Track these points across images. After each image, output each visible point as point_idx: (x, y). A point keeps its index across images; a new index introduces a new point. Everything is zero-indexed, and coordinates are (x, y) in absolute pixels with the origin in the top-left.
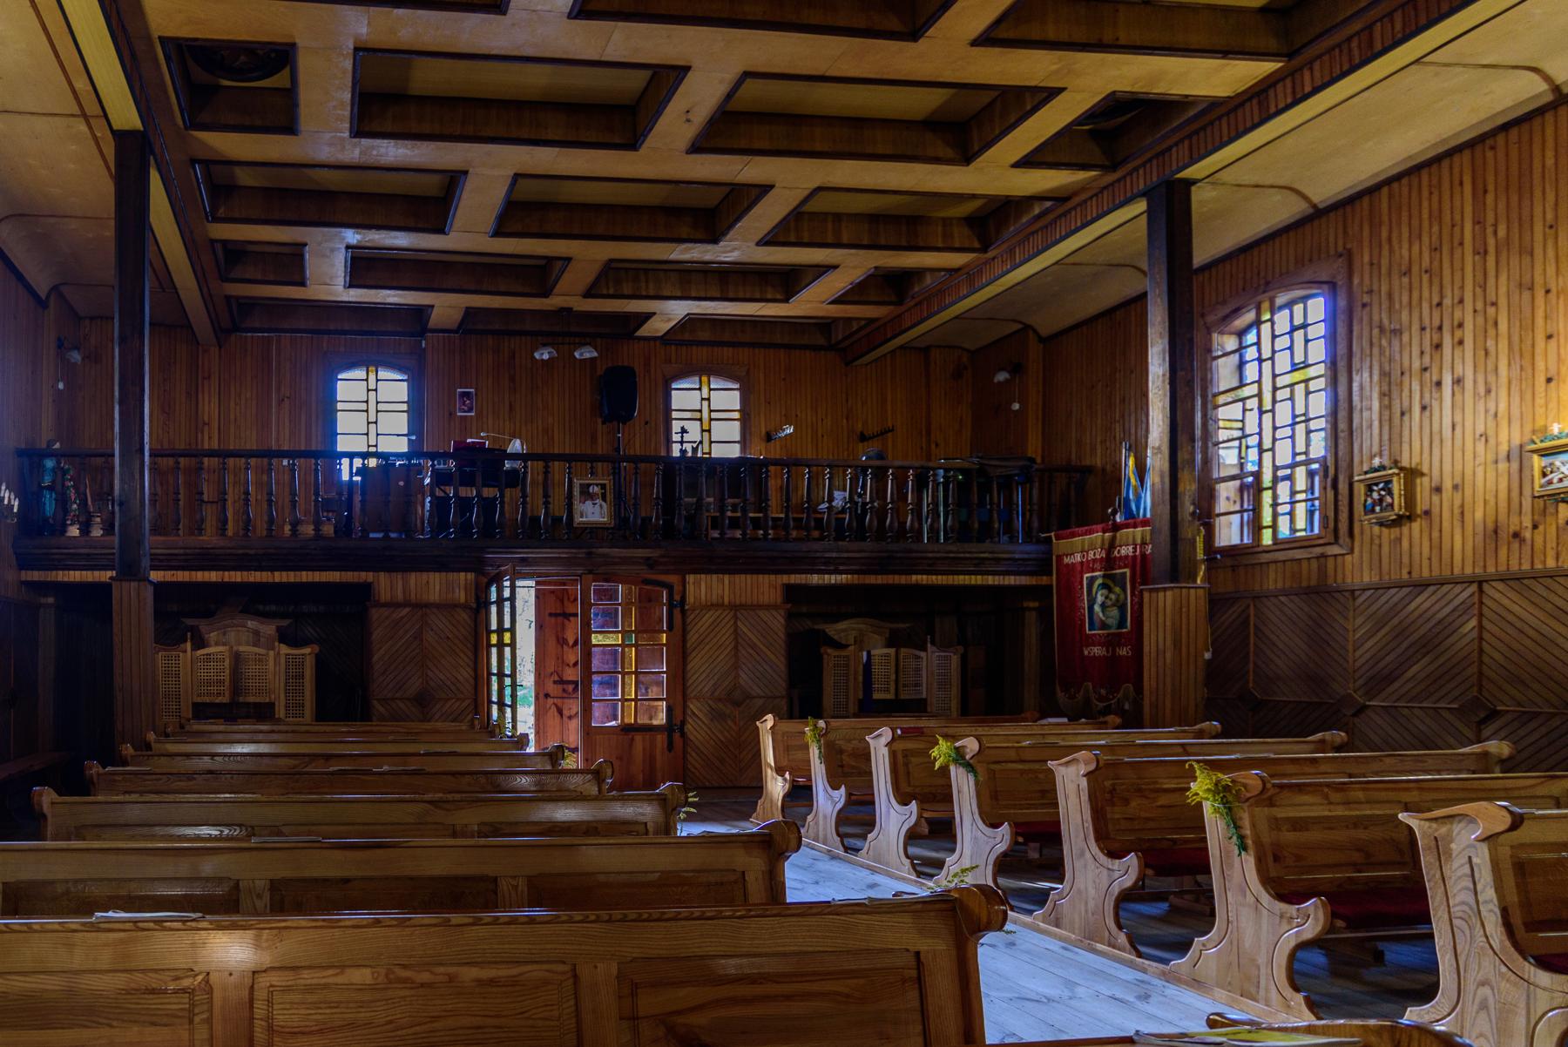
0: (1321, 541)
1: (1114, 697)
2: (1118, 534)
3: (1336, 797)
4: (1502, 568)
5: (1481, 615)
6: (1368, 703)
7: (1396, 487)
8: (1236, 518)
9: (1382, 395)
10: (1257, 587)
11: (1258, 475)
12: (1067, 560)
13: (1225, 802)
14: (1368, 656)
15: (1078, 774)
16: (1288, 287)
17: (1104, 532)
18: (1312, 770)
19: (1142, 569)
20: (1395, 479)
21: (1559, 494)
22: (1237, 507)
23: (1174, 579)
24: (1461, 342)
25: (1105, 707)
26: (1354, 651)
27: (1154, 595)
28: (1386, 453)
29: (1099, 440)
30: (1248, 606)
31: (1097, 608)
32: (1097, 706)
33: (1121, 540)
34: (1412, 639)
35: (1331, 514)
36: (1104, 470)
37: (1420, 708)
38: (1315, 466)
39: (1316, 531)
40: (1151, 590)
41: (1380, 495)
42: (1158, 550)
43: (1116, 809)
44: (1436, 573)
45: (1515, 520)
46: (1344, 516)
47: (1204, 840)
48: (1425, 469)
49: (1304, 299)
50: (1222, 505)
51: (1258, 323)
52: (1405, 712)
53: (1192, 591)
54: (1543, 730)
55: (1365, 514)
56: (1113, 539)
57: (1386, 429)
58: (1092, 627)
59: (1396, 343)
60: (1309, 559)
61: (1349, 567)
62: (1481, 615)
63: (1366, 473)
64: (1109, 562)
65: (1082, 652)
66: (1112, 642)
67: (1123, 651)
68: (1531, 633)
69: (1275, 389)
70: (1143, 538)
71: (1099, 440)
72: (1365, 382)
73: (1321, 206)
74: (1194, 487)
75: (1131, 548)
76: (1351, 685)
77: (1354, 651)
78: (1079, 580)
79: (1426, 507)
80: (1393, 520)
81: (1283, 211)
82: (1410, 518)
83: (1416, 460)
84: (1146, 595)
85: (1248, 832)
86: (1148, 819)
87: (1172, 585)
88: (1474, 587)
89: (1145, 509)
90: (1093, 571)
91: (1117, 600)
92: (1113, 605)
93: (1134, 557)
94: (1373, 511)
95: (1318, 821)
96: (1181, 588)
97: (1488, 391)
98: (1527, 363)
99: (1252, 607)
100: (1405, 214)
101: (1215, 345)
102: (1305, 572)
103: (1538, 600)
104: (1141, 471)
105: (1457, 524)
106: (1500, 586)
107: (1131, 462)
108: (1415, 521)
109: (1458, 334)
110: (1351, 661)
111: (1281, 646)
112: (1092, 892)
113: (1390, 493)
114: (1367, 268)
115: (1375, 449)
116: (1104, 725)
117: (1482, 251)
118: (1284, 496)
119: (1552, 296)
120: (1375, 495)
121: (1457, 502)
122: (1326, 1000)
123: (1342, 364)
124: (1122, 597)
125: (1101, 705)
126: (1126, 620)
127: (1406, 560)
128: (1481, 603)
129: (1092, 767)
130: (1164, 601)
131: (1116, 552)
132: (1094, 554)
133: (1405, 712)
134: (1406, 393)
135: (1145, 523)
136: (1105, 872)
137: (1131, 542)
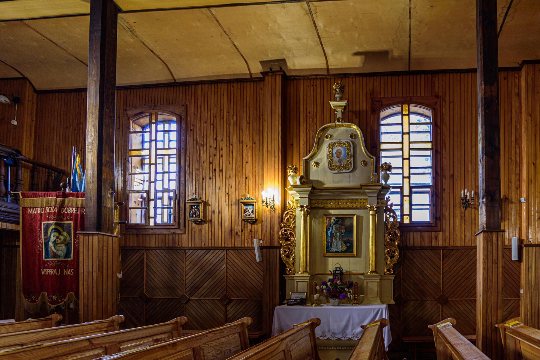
0: (173, 227)
1: (62, 301)
2: (66, 199)
4: (233, 245)
6: (190, 298)
7: (201, 208)
11: (148, 192)
12: (30, 211)
16: (164, 111)
17: (57, 197)
18: (173, 351)
20: (200, 205)
21: (249, 220)
22: (140, 206)
24: (222, 156)
26: (186, 276)
27: (86, 238)
28: (197, 193)
30: (144, 254)
31: (51, 244)
32: (50, 307)
33: (68, 203)
35: (177, 215)
37: (208, 299)
38: (171, 194)
39: (172, 222)
41: (195, 210)
42: (91, 212)
44: (213, 245)
45: (236, 227)
46: (182, 218)
48: (210, 203)
50: (133, 205)
51: (151, 123)
52: (203, 301)
53: (110, 238)
54: (244, 306)
55: (190, 218)
56: (63, 202)
57: (197, 183)
58: (47, 256)
60: (169, 234)
61: (184, 239)
62: (227, 263)
63: (190, 200)
64: (60, 216)
66: (60, 266)
67: (69, 272)
68: (241, 270)
69: (156, 155)
70: (82, 204)
73: (177, 81)
75: (74, 209)
76: (184, 291)
77: (186, 276)
78: (38, 225)
79: (210, 218)
80: (199, 222)
81: (162, 77)
83: (207, 199)
84: (81, 237)
87: (97, 232)
88: (225, 252)
91: (65, 240)
92: (62, 243)
94: (193, 216)
96: (103, 235)
97: (230, 177)
99: (145, 254)
100: (206, 99)
102: (167, 241)
103: (243, 258)
107: (78, 159)
108: (207, 223)
109: (221, 152)
110: (184, 280)
111: (158, 273)
113: (198, 210)
114: (193, 115)
115: (194, 191)
117: (229, 124)
119: (248, 147)
120: (193, 210)
124: (68, 238)
125: (53, 306)
126: (71, 252)
127: (203, 238)
128: (227, 258)
131: (65, 210)
132: (50, 210)
133: (203, 301)
135: (83, 195)
137: (74, 205)
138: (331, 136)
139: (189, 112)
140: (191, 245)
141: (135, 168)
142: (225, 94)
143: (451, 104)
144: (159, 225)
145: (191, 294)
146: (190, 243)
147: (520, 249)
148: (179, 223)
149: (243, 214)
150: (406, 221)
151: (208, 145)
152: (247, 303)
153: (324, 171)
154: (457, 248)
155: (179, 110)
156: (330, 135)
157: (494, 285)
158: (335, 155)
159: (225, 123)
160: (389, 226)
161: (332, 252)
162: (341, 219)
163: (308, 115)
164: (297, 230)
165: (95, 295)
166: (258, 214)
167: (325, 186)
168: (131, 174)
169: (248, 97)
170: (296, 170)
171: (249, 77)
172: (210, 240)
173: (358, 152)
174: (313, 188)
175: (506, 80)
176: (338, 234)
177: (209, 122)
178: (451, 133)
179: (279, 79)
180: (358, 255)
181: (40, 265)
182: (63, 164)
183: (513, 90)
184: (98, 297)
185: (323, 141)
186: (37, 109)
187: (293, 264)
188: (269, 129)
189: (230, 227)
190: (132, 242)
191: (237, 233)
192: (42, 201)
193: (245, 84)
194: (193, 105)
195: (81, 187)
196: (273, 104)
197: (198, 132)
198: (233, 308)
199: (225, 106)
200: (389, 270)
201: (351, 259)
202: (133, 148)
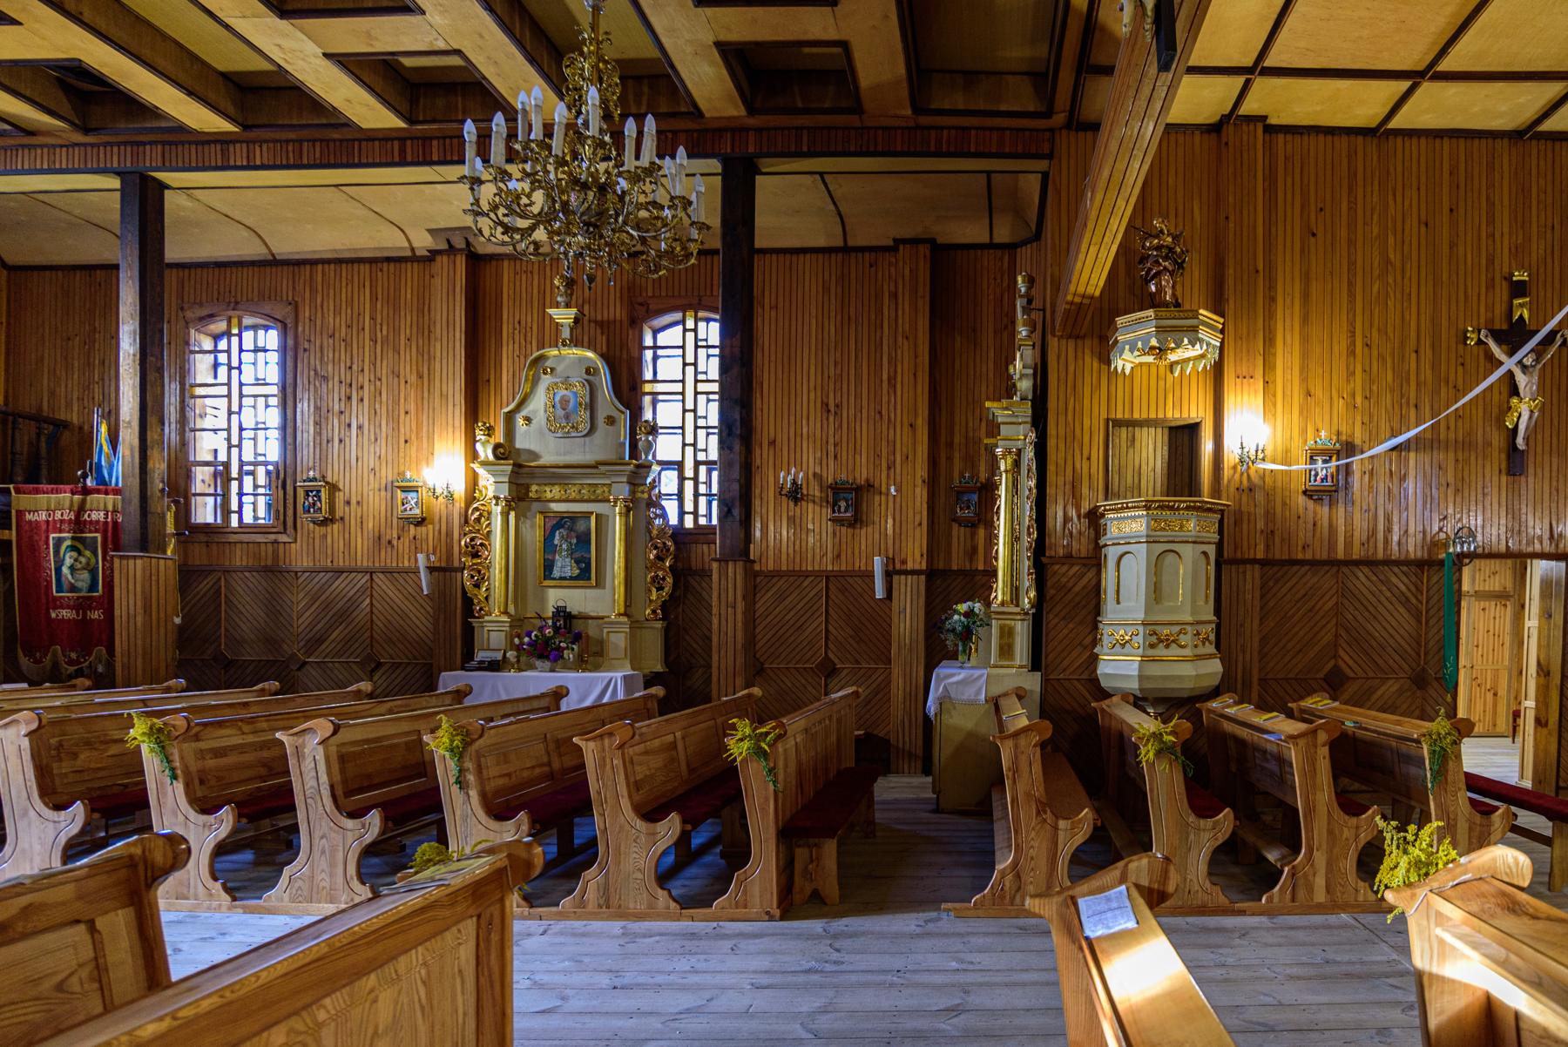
2: (88, 498)
3: (246, 728)
5: (372, 596)
8: (210, 500)
9: (316, 423)
10: (227, 563)
11: (227, 465)
12: (29, 517)
13: (159, 742)
14: (306, 623)
15: (18, 735)
16: (254, 313)
19: (113, 535)
22: (211, 491)
23: (144, 548)
24: (362, 400)
25: (76, 671)
27: (124, 562)
29: (75, 397)
31: (65, 570)
34: (335, 610)
36: (81, 428)
38: (270, 468)
40: (121, 557)
42: (130, 521)
43: (64, 764)
45: (389, 531)
46: (290, 512)
47: (144, 782)
48: (341, 487)
49: (266, 328)
50: (198, 487)
51: (228, 334)
53: (162, 562)
56: (83, 502)
59: (324, 386)
61: (293, 551)
64: (79, 524)
65: (48, 614)
66: (82, 605)
67: (95, 615)
71: (75, 397)
72: (304, 408)
73: (278, 257)
74: (164, 466)
75: (102, 514)
78: (43, 538)
81: (253, 250)
82: (332, 521)
83: (335, 478)
84: (117, 561)
85: (177, 764)
86: (99, 769)
88: (368, 576)
89: (117, 478)
90: (60, 532)
91: (88, 564)
93: (106, 523)
95: (234, 748)
97: (376, 440)
98: (395, 425)
100: (332, 292)
101: (192, 341)
102: (263, 554)
104: (114, 441)
105: (359, 530)
106: (381, 575)
107: (104, 429)
109: (361, 392)
112: (37, 848)
113: (320, 500)
114: (307, 321)
115: (311, 464)
116: (74, 687)
118: (248, 488)
121: (359, 515)
122: (246, 884)
123: (289, 390)
124: (93, 560)
125: (72, 669)
127: (329, 552)
129: (34, 726)
130: (133, 570)
131: (86, 516)
134: (330, 427)
135: (117, 492)
136: (51, 825)
138: (552, 369)
139: (301, 317)
140: (306, 563)
141: (201, 416)
142: (367, 284)
143: (773, 313)
144: (249, 526)
145: (309, 653)
146: (305, 559)
147: (889, 575)
148: (285, 522)
149: (401, 508)
150: (689, 522)
151: (336, 379)
152: (409, 669)
153: (541, 434)
154: (777, 574)
155: (281, 311)
156: (552, 369)
157: (730, 640)
158: (558, 406)
159: (367, 341)
160: (655, 532)
161: (554, 579)
162: (564, 522)
163: (517, 326)
164: (492, 537)
165: (140, 651)
166: (428, 508)
167: (541, 462)
168: (194, 430)
169: (409, 291)
170: (490, 431)
171: (409, 254)
172: (341, 555)
173: (600, 399)
174: (518, 466)
175: (873, 269)
176: (564, 546)
177: (337, 335)
178: (772, 365)
179: (461, 262)
180: (599, 584)
181: (48, 603)
182: (63, 409)
183: (886, 287)
184: (144, 653)
185: (539, 379)
186: (8, 301)
187: (487, 598)
188: (445, 354)
189: (376, 530)
190: (199, 556)
191: (390, 542)
192: (49, 501)
193: (403, 265)
194: (307, 301)
195: (110, 476)
196: (451, 308)
197: (318, 355)
198: (384, 678)
199: (367, 306)
200: (654, 612)
201: (588, 591)
202: (198, 382)
